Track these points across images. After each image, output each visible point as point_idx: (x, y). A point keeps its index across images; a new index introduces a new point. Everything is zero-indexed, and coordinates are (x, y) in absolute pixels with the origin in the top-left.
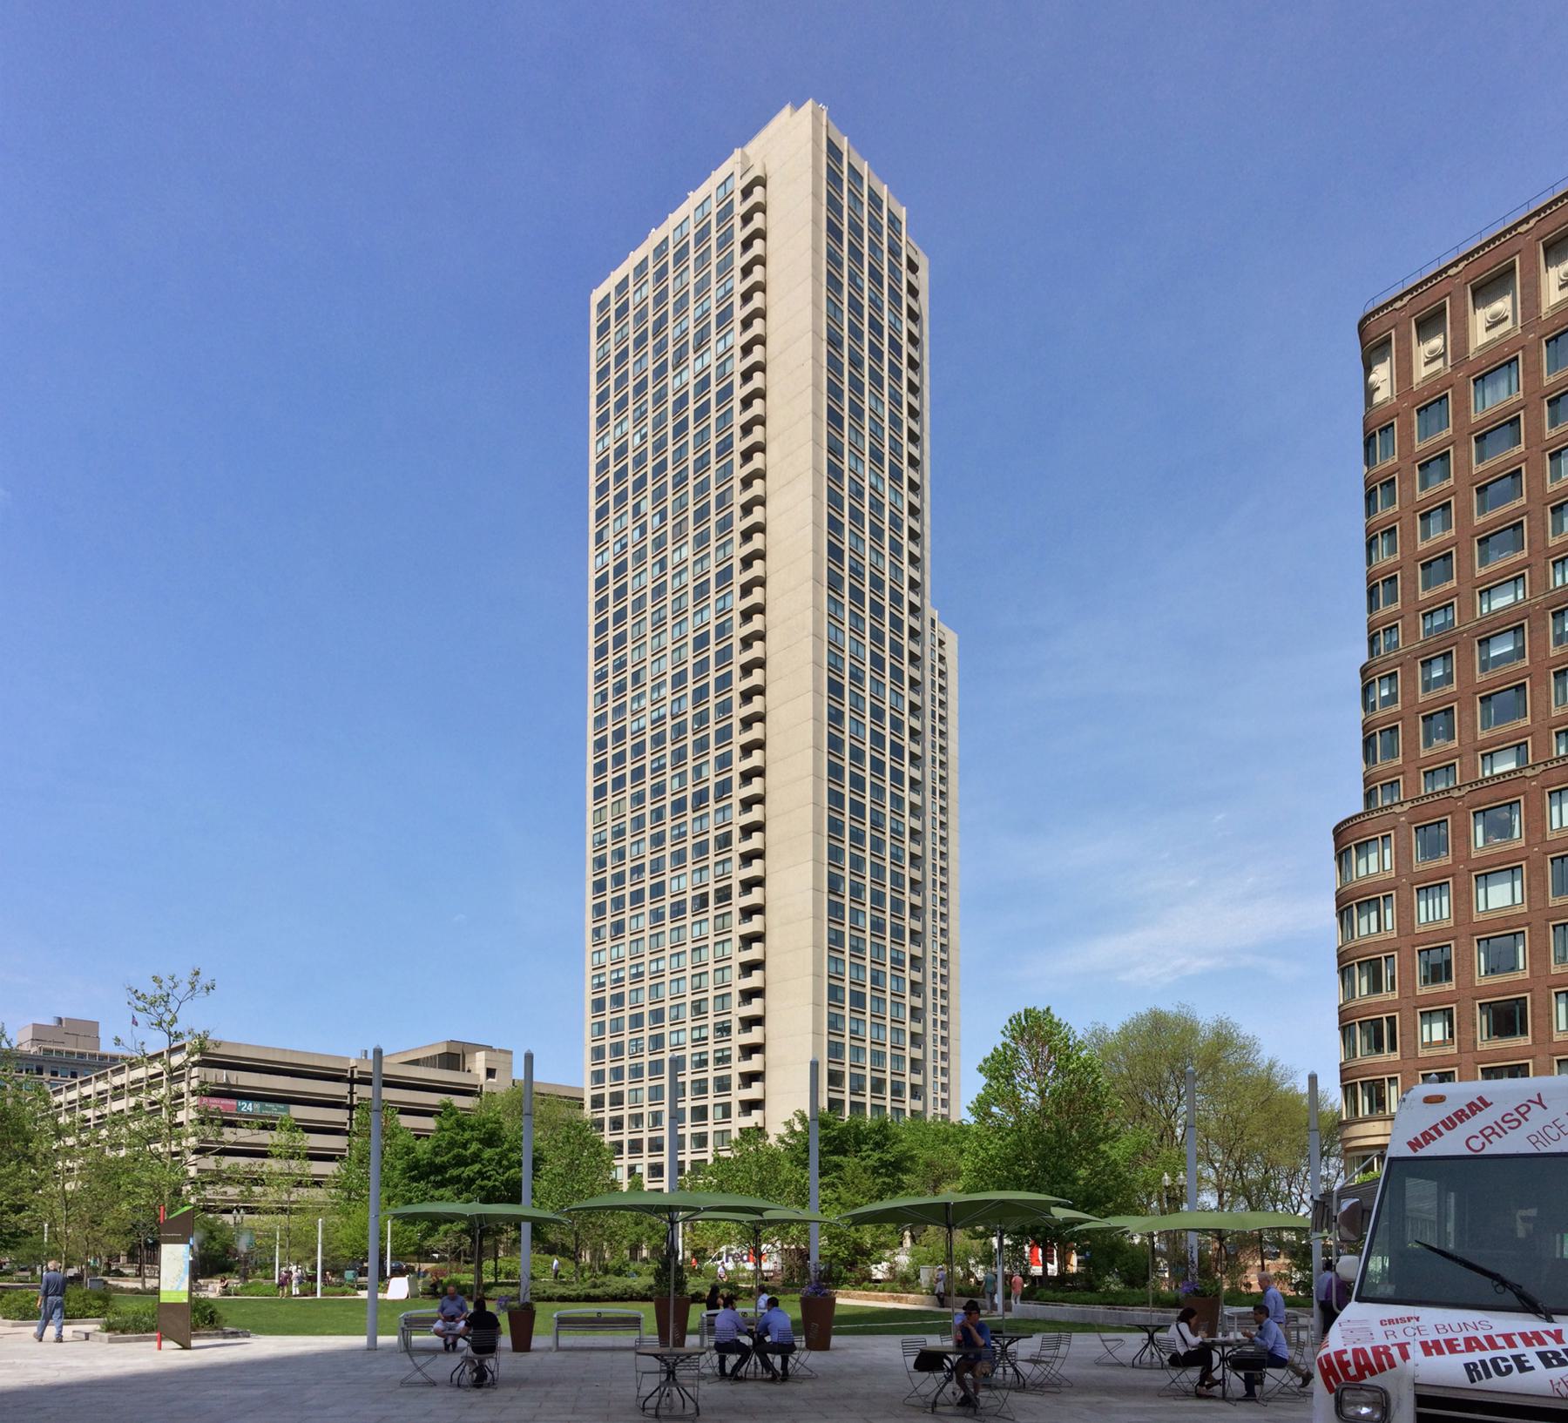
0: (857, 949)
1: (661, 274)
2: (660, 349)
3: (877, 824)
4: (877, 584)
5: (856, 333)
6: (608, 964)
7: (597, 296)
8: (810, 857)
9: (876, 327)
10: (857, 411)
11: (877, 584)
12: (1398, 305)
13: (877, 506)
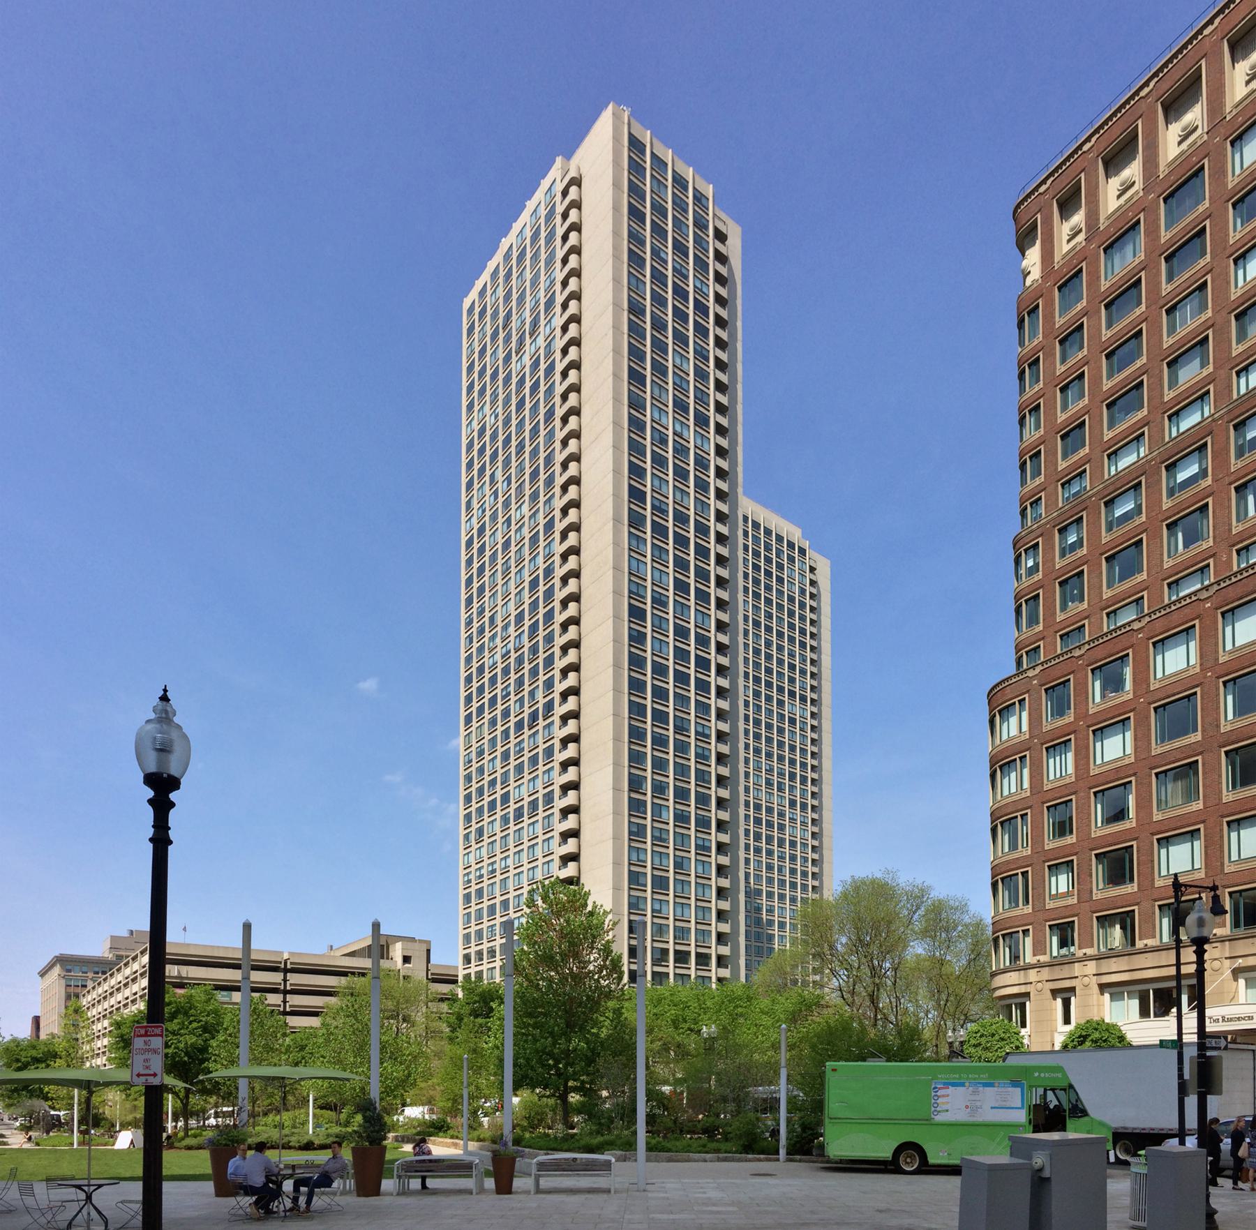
0: (660, 839)
1: (508, 276)
2: (507, 339)
3: (681, 728)
4: (681, 518)
5: (659, 300)
6: (473, 864)
7: (467, 303)
8: (611, 762)
9: (680, 293)
10: (660, 370)
11: (681, 518)
12: (1042, 189)
13: (681, 451)
